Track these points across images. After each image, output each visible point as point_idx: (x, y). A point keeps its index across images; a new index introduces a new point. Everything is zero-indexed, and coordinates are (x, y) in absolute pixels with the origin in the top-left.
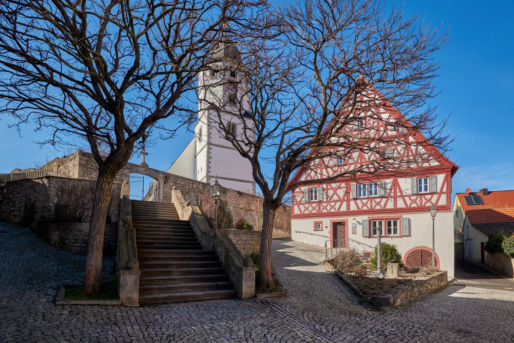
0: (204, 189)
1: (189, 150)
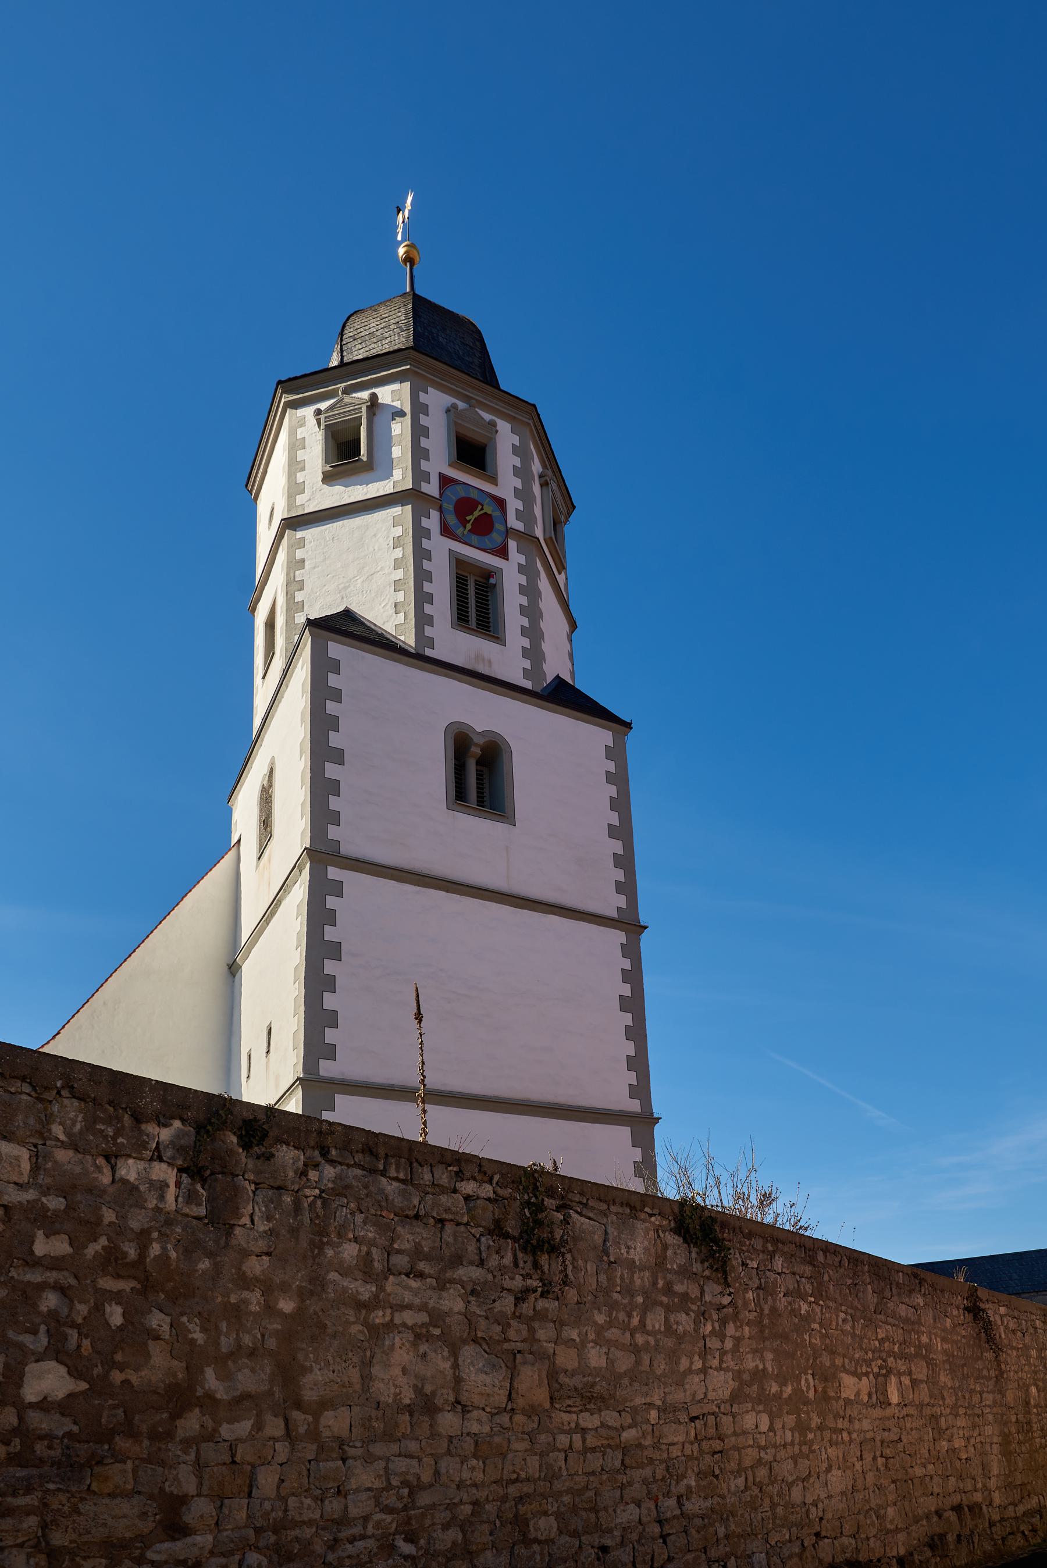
0: (221, 1218)
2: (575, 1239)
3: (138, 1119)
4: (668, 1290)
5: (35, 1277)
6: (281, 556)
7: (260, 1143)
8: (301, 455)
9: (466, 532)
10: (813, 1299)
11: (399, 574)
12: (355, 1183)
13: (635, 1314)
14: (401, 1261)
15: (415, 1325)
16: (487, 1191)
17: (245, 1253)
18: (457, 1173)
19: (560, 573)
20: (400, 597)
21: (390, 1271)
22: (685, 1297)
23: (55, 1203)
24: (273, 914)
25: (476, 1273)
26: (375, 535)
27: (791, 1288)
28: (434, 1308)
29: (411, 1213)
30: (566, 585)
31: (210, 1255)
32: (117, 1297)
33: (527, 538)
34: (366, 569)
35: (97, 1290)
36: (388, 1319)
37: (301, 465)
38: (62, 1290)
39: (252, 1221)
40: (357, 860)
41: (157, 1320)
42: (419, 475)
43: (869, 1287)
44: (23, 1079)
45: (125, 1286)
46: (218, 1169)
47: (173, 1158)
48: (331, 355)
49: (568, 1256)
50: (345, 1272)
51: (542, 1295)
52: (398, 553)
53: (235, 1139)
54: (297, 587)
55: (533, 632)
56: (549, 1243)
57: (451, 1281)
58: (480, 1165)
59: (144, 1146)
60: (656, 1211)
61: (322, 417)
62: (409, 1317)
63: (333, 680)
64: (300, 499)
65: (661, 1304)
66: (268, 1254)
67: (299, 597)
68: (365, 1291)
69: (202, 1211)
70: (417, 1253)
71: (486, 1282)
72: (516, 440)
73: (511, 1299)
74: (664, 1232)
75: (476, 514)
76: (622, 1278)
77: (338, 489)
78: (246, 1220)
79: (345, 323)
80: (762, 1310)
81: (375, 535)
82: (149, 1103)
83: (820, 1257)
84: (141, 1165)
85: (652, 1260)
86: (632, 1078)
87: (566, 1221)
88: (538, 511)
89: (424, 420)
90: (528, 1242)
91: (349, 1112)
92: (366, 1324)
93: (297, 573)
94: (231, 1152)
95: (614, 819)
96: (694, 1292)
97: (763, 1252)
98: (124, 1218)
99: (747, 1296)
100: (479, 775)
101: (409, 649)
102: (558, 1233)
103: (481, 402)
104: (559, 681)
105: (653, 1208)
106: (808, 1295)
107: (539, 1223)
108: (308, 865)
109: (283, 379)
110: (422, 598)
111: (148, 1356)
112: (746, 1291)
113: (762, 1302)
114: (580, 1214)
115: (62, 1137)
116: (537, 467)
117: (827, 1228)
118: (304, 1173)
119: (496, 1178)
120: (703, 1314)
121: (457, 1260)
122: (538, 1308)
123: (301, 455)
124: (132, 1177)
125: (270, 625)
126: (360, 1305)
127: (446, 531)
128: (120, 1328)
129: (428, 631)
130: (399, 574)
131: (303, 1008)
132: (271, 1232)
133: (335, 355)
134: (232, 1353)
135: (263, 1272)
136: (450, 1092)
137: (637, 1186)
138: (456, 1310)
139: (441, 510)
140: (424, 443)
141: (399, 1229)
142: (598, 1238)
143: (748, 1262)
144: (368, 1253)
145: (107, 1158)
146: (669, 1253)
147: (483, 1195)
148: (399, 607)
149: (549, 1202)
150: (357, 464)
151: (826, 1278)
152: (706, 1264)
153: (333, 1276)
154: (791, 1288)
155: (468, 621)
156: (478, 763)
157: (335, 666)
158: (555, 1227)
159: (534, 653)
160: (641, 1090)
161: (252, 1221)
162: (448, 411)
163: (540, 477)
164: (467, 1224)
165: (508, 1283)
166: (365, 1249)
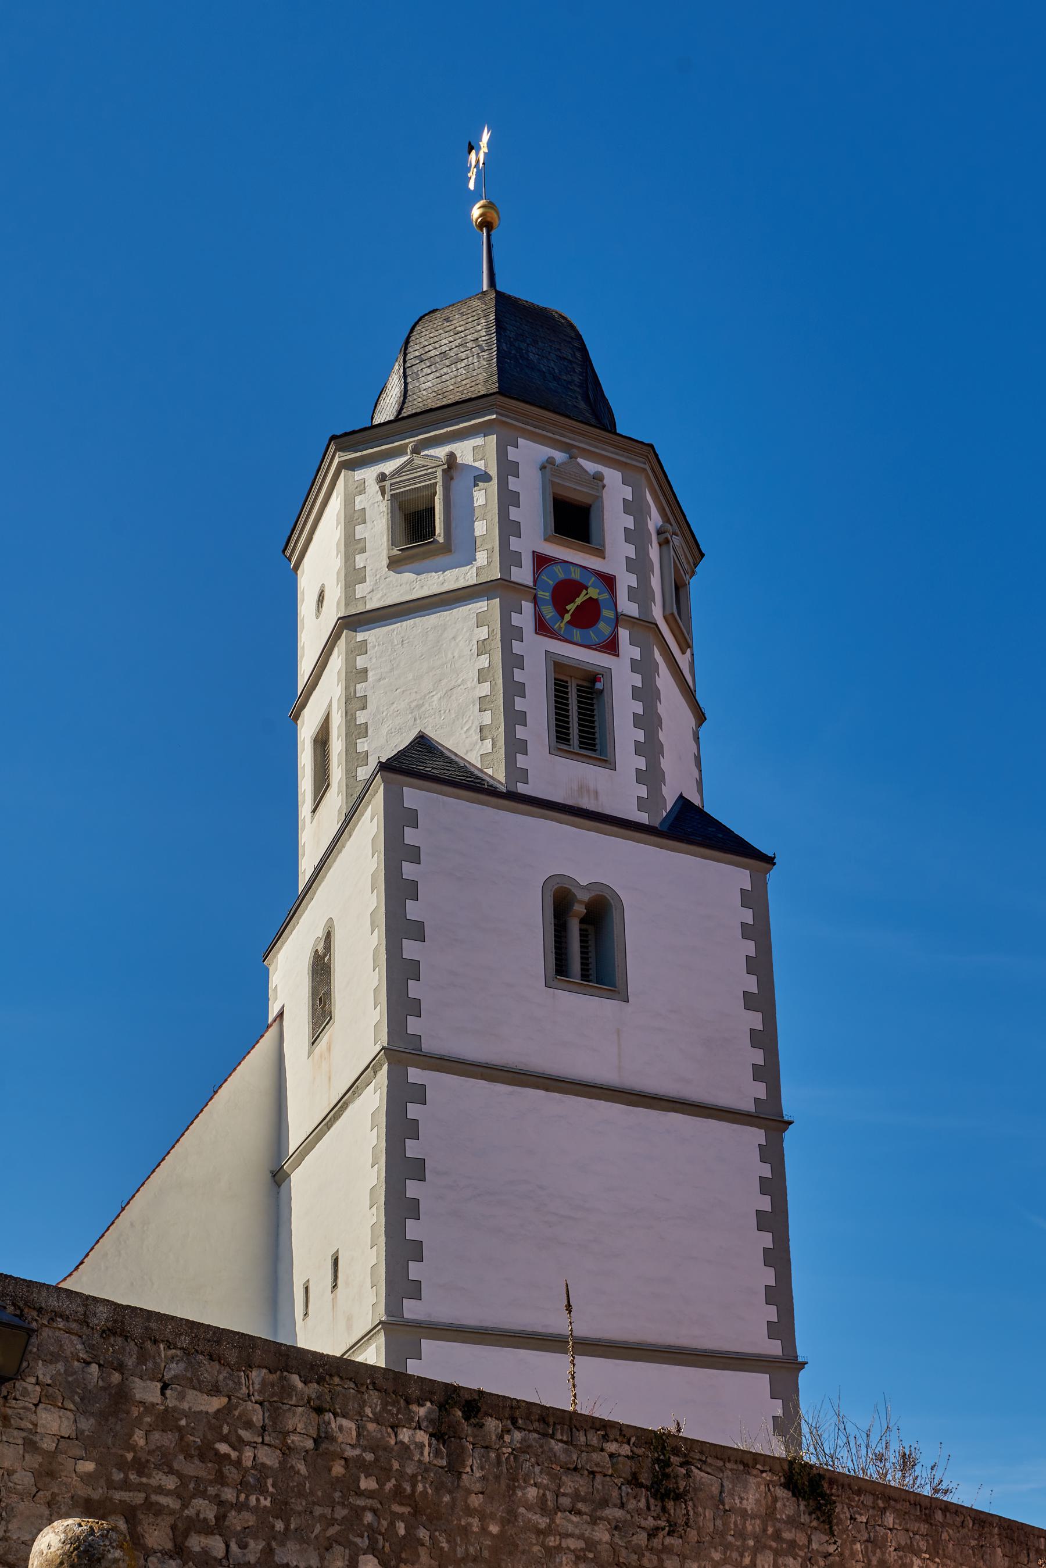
0: (454, 1469)
1: (234, 1105)
2: (695, 1490)
3: (408, 1402)
4: (777, 1536)
5: (361, 1502)
6: (337, 662)
7: (475, 1416)
8: (360, 531)
9: (562, 625)
10: (927, 1556)
11: (485, 689)
12: (534, 1444)
13: (746, 1554)
14: (566, 1501)
15: (576, 1549)
16: (626, 1450)
17: (469, 1492)
18: (604, 1436)
19: (683, 653)
20: (487, 718)
21: (558, 1508)
22: (793, 1544)
23: (369, 1457)
24: (336, 1117)
25: (618, 1513)
26: (454, 638)
27: (903, 1543)
28: (589, 1538)
29: (572, 1466)
30: (692, 665)
31: (450, 1492)
32: (401, 1517)
33: (644, 625)
34: (444, 682)
35: (391, 1512)
36: (557, 1543)
37: (361, 545)
38: (374, 1511)
39: (472, 1470)
40: (441, 1058)
41: (423, 1533)
42: (509, 558)
43: (999, 1550)
44: (351, 1380)
45: (405, 1510)
46: (452, 1434)
47: (427, 1427)
48: (388, 375)
49: (690, 1503)
50: (529, 1508)
51: (669, 1534)
52: (484, 661)
53: (460, 1414)
54: (359, 705)
55: (650, 748)
56: (674, 1491)
57: (601, 1518)
58: (621, 1430)
59: (412, 1419)
60: (767, 1468)
61: (387, 484)
62: (572, 1543)
63: (411, 837)
64: (360, 590)
65: (770, 1548)
66: (482, 1493)
67: (361, 717)
68: (543, 1522)
69: (444, 1463)
70: (576, 1496)
71: (625, 1521)
72: (628, 493)
73: (644, 1535)
74: (774, 1486)
75: (579, 601)
76: (735, 1523)
77: (408, 576)
78: (468, 1469)
79: (409, 337)
80: (870, 1561)
81: (454, 638)
82: (414, 1391)
83: (939, 1516)
84: (410, 1432)
85: (763, 1511)
86: (771, 1313)
87: (688, 1475)
88: (655, 582)
89: (513, 484)
90: (657, 1491)
91: (439, 1363)
92: (543, 1545)
93: (359, 686)
94: (458, 1423)
95: (751, 984)
96: (802, 1539)
97: (874, 1508)
98: (404, 1466)
99: (855, 1547)
100: (584, 940)
101: (498, 785)
102: (682, 1484)
103: (584, 449)
104: (684, 804)
105: (763, 1466)
106: (921, 1551)
107: (667, 1476)
108: (385, 1067)
109: (338, 433)
110: (514, 718)
111: (419, 1556)
112: (854, 1542)
113: (870, 1554)
114: (700, 1469)
115: (370, 1415)
116: (655, 520)
117: (964, 1494)
118: (501, 1437)
119: (633, 1439)
120: (810, 1560)
121: (605, 1503)
122: (666, 1543)
123: (360, 531)
124: (406, 1440)
125: (322, 741)
126: (539, 1532)
127: (542, 627)
128: (404, 1537)
129: (521, 761)
130: (485, 689)
131: (382, 1239)
132: (484, 1478)
133: (396, 367)
134: (463, 1558)
135: (480, 1505)
136: (552, 1335)
137: (778, 1449)
138: (604, 1540)
139: (535, 600)
140: (514, 514)
141: (564, 1478)
142: (715, 1490)
143: (857, 1516)
144: (544, 1495)
145: (392, 1427)
146: (779, 1505)
147: (623, 1453)
148: (486, 732)
149: (673, 1459)
150: (432, 546)
151: (945, 1536)
152: (814, 1516)
153: (522, 1510)
154: (903, 1543)
155: (568, 740)
156: (582, 921)
157: (412, 818)
158: (679, 1479)
159: (651, 776)
160: (783, 1328)
161: (472, 1470)
162: (543, 468)
163: (659, 532)
164: (611, 1476)
165: (643, 1523)
166: (541, 1491)
